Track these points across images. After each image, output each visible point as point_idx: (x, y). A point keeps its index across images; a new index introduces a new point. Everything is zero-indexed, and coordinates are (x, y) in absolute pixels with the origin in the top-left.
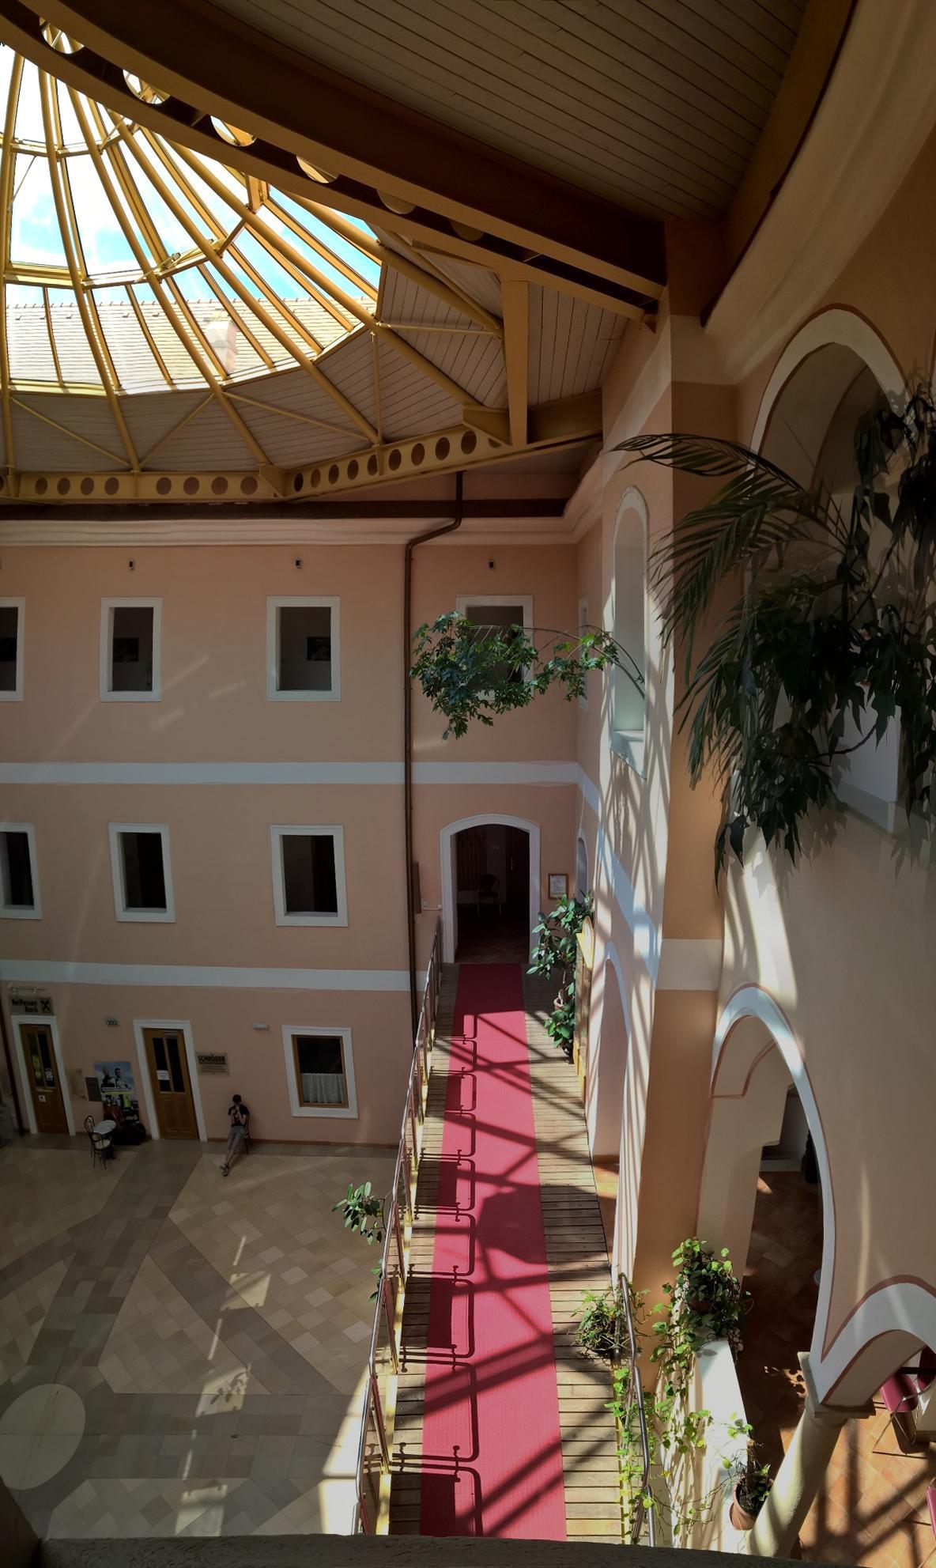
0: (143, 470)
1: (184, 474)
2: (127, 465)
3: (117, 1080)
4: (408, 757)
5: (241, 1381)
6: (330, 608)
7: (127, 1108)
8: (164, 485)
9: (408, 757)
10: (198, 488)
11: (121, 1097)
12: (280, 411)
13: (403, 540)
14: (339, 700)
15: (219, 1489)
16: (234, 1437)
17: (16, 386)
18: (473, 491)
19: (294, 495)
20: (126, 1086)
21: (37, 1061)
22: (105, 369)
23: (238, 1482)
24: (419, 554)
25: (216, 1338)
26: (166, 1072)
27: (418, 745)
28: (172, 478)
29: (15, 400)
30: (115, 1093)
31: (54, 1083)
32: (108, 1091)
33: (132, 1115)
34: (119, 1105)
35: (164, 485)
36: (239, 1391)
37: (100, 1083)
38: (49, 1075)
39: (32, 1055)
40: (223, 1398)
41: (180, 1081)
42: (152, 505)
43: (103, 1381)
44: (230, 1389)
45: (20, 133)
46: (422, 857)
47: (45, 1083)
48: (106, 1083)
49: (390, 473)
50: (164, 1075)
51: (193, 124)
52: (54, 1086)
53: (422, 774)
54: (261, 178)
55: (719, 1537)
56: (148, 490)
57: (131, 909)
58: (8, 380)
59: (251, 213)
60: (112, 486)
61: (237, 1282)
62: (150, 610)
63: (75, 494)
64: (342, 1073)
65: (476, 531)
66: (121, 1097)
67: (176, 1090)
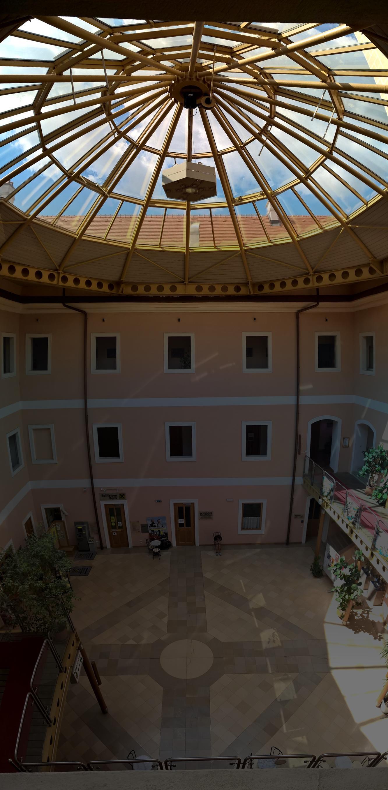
0: (189, 282)
1: (208, 284)
2: (183, 280)
3: (158, 524)
4: (298, 393)
6: (48, 338)
7: (161, 535)
8: (199, 289)
9: (298, 393)
10: (263, 290)
11: (159, 531)
12: (269, 259)
13: (295, 310)
14: (340, 371)
17: (165, 249)
18: (321, 293)
19: (258, 293)
20: (162, 526)
21: (113, 519)
24: (301, 316)
25: (255, 619)
26: (183, 520)
27: (301, 388)
28: (203, 286)
29: (136, 253)
30: (156, 530)
31: (124, 527)
32: (153, 529)
33: (164, 538)
34: (158, 534)
35: (199, 289)
37: (149, 525)
38: (120, 524)
39: (110, 517)
41: (189, 523)
42: (154, 297)
45: (220, 147)
46: (300, 432)
47: (117, 527)
48: (152, 525)
49: (61, 283)
50: (181, 521)
52: (122, 528)
53: (304, 400)
56: (191, 290)
57: (247, 456)
58: (243, 246)
59: (306, 181)
60: (173, 289)
62: (247, 337)
63: (154, 291)
64: (260, 516)
65: (324, 307)
66: (159, 531)
67: (186, 527)
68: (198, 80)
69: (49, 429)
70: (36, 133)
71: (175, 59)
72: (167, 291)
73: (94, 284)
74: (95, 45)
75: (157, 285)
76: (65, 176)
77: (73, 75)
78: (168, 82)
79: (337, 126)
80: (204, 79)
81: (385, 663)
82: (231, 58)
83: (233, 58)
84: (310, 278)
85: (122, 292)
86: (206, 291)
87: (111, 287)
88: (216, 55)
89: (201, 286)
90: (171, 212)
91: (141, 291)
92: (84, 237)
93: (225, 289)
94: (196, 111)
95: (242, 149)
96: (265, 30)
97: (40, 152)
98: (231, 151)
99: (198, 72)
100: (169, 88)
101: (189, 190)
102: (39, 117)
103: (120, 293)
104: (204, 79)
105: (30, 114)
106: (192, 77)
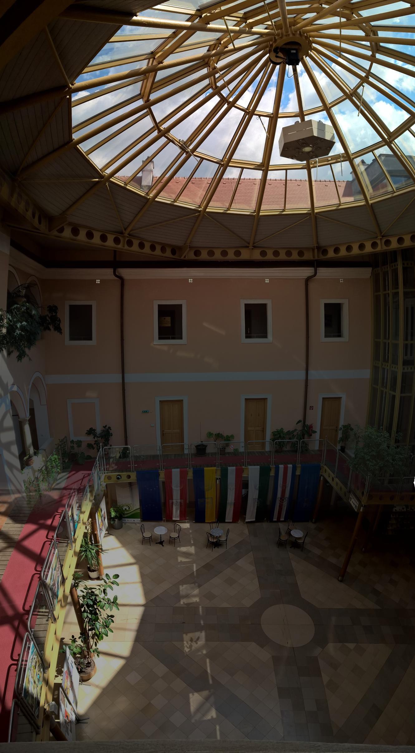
5: (188, 648)
8: (263, 253)
15: (184, 603)
16: (184, 623)
19: (322, 257)
22: (216, 181)
23: (177, 605)
25: (209, 671)
28: (267, 251)
35: (263, 253)
36: (187, 643)
40: (194, 640)
43: (206, 521)
44: (192, 644)
49: (126, 247)
51: (81, 675)
54: (69, 106)
55: (74, 474)
56: (257, 256)
60: (238, 253)
61: (208, 710)
63: (218, 256)
68: (294, 34)
69: (181, 401)
70: (148, 119)
71: (262, 23)
72: (231, 256)
73: (158, 248)
74: (186, 31)
75: (273, 250)
76: (183, 152)
77: (339, 30)
78: (264, 45)
79: (370, 62)
80: (300, 32)
81: (108, 553)
82: (320, 6)
83: (322, 5)
84: (378, 242)
85: (185, 257)
86: (270, 256)
87: (173, 252)
88: (270, 14)
89: (278, 251)
90: (292, 174)
91: (204, 256)
92: (209, 209)
93: (289, 253)
94: (300, 67)
95: (353, 97)
96: (207, 5)
97: (155, 133)
98: (338, 102)
99: (293, 27)
100: (268, 50)
101: (307, 149)
102: (148, 105)
103: (182, 258)
104: (300, 32)
105: (140, 103)
106: (288, 34)
